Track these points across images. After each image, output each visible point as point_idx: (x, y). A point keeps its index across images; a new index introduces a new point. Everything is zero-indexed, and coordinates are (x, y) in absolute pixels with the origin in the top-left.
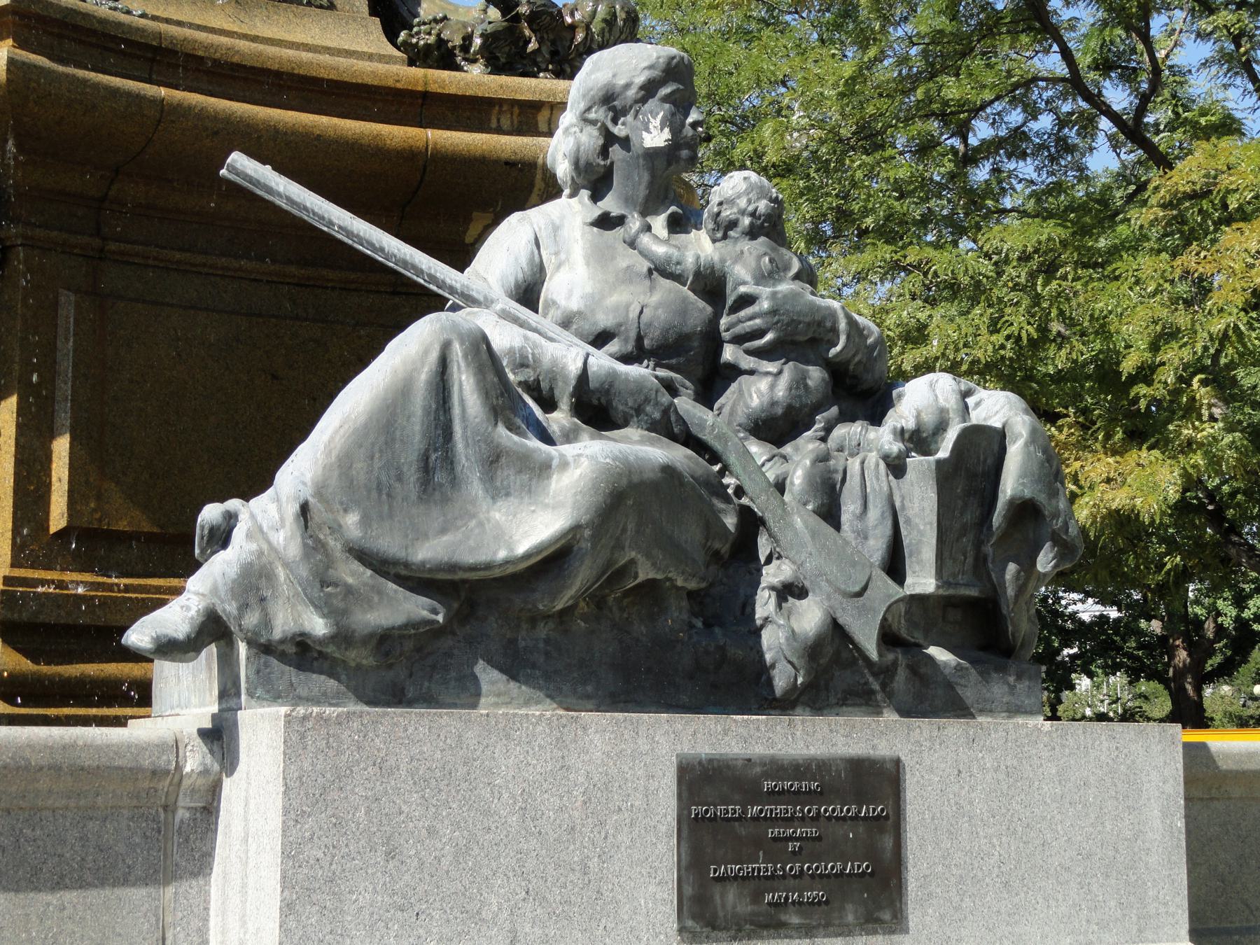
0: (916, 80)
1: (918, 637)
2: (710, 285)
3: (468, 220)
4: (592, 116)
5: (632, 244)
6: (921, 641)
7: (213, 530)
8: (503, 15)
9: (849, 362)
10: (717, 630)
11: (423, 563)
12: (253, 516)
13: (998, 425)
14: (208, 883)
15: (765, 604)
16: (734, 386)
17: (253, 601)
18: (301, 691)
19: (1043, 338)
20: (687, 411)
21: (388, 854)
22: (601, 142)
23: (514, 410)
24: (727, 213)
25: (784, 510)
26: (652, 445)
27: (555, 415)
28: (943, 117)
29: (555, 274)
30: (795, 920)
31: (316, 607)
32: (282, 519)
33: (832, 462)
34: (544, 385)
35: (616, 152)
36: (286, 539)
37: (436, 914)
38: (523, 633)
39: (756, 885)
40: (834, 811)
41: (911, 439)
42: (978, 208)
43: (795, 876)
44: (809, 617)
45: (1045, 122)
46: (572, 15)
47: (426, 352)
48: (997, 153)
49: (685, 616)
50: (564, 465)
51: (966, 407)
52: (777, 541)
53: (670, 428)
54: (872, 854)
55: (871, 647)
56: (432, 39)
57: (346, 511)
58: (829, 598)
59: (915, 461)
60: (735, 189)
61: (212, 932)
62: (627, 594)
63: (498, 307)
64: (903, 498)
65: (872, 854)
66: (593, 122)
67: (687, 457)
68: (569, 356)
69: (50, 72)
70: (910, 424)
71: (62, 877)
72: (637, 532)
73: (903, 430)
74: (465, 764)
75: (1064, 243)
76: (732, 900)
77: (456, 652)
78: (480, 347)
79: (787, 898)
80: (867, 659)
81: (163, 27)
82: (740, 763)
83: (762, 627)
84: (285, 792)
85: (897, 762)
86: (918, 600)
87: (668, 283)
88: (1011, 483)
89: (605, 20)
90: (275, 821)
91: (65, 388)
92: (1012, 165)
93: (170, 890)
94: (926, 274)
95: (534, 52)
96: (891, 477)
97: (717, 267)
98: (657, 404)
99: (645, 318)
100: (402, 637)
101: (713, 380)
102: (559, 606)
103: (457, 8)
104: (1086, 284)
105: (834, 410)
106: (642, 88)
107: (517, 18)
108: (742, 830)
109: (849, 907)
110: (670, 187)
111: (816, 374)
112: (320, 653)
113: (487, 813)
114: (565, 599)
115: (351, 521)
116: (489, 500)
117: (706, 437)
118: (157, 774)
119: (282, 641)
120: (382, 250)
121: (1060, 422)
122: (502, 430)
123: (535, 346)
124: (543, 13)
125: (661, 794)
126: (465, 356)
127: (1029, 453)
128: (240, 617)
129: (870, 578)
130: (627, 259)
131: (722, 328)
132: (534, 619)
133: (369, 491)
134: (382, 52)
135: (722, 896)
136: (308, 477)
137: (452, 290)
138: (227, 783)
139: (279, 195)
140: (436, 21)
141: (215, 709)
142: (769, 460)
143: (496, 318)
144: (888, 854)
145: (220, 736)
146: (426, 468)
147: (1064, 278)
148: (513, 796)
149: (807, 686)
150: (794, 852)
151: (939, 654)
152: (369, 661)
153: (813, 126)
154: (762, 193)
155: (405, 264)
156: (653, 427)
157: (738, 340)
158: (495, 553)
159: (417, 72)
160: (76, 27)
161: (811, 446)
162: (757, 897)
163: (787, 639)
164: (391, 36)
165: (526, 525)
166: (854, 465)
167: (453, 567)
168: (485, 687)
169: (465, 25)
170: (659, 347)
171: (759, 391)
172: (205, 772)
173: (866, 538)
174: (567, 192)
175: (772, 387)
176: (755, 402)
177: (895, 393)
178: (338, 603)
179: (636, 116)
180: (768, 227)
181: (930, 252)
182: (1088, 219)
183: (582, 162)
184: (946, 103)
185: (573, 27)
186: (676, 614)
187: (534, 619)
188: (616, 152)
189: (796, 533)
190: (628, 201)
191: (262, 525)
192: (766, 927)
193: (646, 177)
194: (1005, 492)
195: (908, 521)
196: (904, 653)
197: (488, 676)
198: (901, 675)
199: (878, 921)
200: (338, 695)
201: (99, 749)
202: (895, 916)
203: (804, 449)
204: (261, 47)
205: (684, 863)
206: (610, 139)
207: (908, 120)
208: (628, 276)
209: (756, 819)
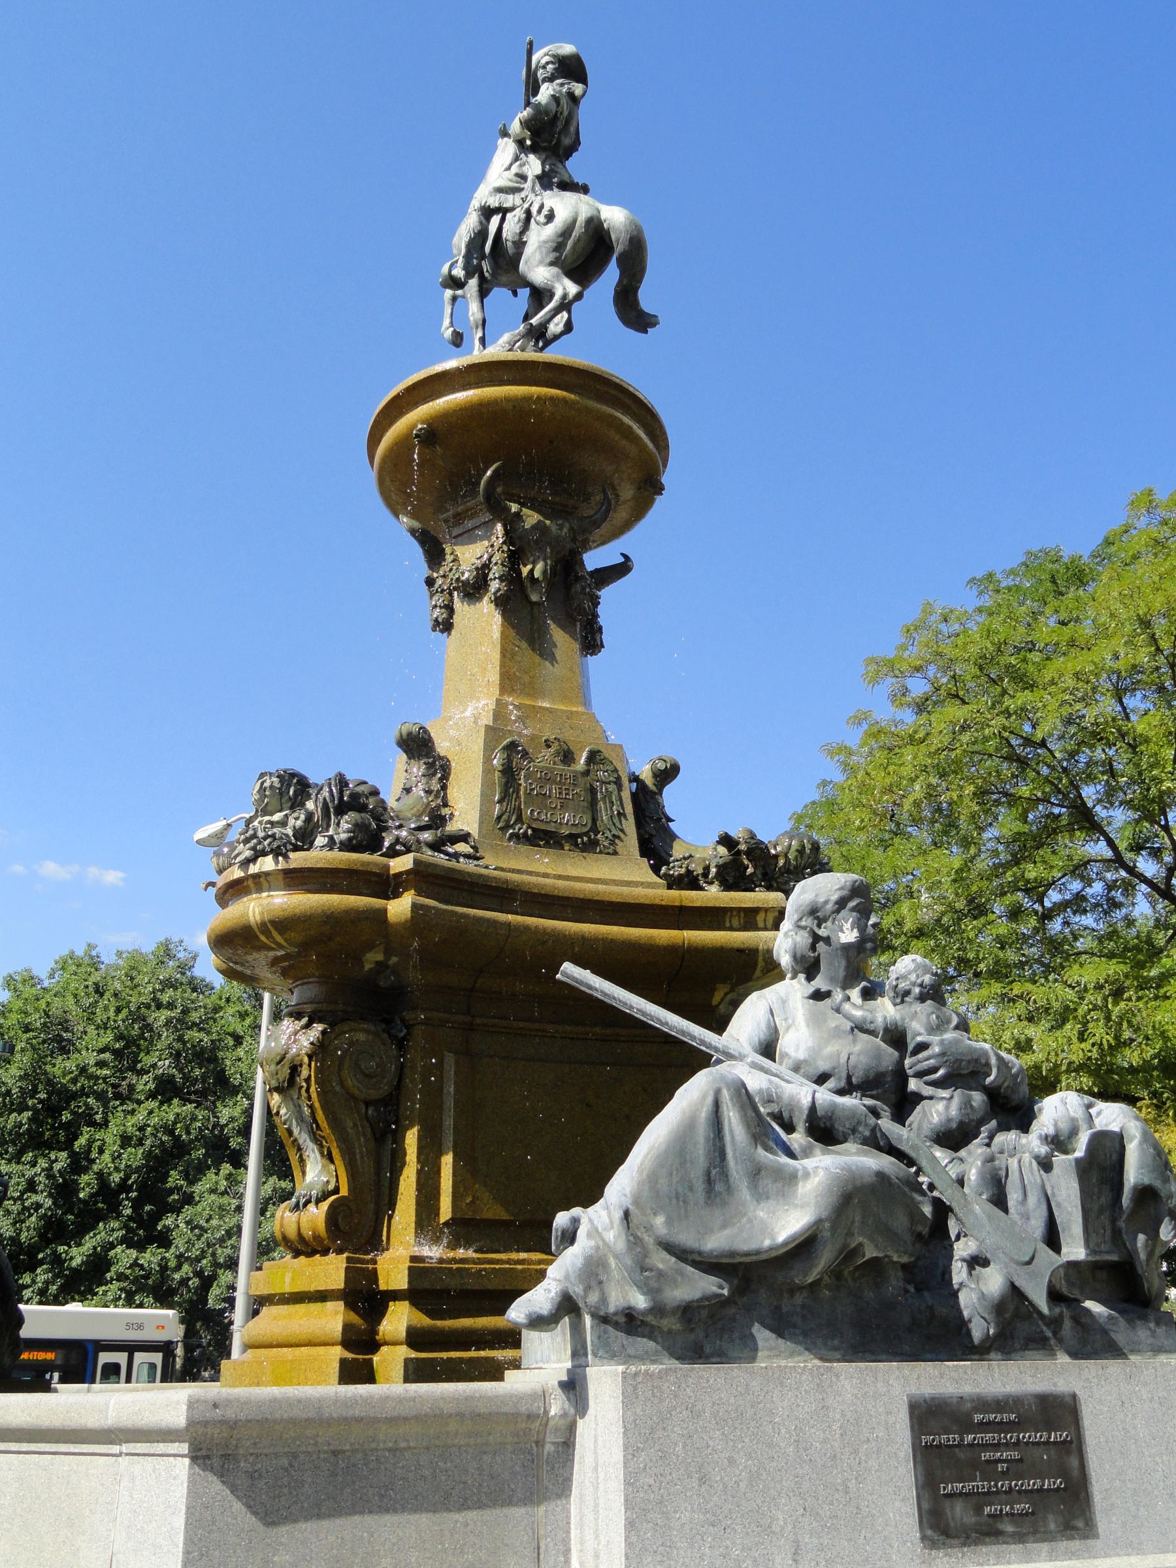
0: (1006, 866)
1: (1076, 1294)
2: (896, 1037)
3: (713, 990)
4: (803, 923)
5: (838, 1010)
6: (1079, 1297)
7: (564, 1232)
8: (729, 851)
9: (1000, 1087)
10: (926, 1293)
11: (711, 1251)
12: (591, 1220)
13: (1117, 1129)
14: (569, 1503)
15: (959, 1273)
16: (919, 1108)
17: (593, 1283)
18: (631, 1351)
19: (1121, 1043)
20: (888, 1129)
21: (700, 1480)
22: (810, 940)
23: (766, 1135)
24: (903, 985)
25: (966, 1200)
26: (866, 1155)
27: (794, 1135)
28: (1027, 891)
29: (785, 1034)
30: (1010, 1529)
31: (638, 1287)
32: (611, 1222)
33: (997, 1162)
34: (786, 1115)
35: (821, 946)
36: (614, 1236)
37: (739, 1528)
38: (785, 1301)
39: (978, 1500)
40: (1030, 1437)
41: (1052, 1142)
42: (1059, 952)
43: (1005, 1492)
44: (993, 1281)
45: (1098, 888)
46: (775, 848)
47: (704, 1097)
48: (1065, 911)
49: (901, 1284)
50: (807, 1175)
51: (1091, 1116)
52: (962, 1223)
53: (879, 1143)
54: (1064, 1473)
55: (1043, 1305)
56: (683, 871)
57: (655, 1214)
58: (1006, 1267)
59: (1059, 1159)
60: (908, 967)
61: (573, 1542)
62: (858, 1268)
63: (749, 1060)
64: (1053, 1188)
65: (1064, 1473)
66: (804, 928)
67: (891, 1163)
68: (802, 1094)
69: (437, 910)
70: (1051, 1131)
71: (466, 1499)
72: (863, 1223)
73: (1046, 1136)
74: (752, 1406)
75: (1126, 976)
76: (959, 1512)
77: (738, 1317)
78: (741, 1092)
79: (1001, 1510)
80: (1039, 1313)
81: (509, 875)
82: (955, 1400)
83: (959, 1290)
84: (624, 1433)
85: (1074, 1396)
86: (1072, 1265)
87: (865, 1037)
88: (1133, 1174)
89: (797, 851)
90: (618, 1455)
91: (449, 1122)
92: (1077, 919)
93: (542, 1508)
94: (1028, 1002)
95: (751, 874)
96: (1042, 1172)
97: (899, 1023)
98: (866, 1125)
99: (851, 1062)
100: (699, 1307)
101: (904, 1105)
102: (810, 1281)
103: (697, 847)
104: (1147, 1003)
105: (994, 1123)
106: (837, 903)
107: (739, 852)
108: (961, 1454)
109: (1051, 1517)
110: (858, 968)
111: (978, 1098)
112: (642, 1321)
113: (770, 1445)
114: (815, 1274)
115: (659, 1221)
116: (755, 1202)
117: (903, 1147)
118: (531, 1417)
119: (616, 1314)
120: (667, 1024)
121: (1138, 1104)
122: (761, 1151)
123: (777, 1087)
124: (757, 848)
125: (898, 1426)
126: (731, 1099)
127: (1143, 1150)
128: (586, 1296)
129: (1035, 1251)
130: (835, 1021)
131: (907, 1066)
132: (793, 1290)
133: (670, 1199)
134: (649, 880)
135: (952, 1508)
136: (628, 1191)
137: (716, 1050)
138: (580, 1423)
139: (596, 990)
140: (685, 858)
141: (569, 1365)
142: (950, 1162)
143: (748, 1068)
144: (1076, 1473)
145: (574, 1386)
146: (709, 1181)
147: (1130, 999)
148: (789, 1432)
149: (998, 1336)
150: (1002, 1472)
151: (1094, 1307)
152: (677, 1326)
153: (936, 904)
154: (926, 970)
155: (683, 1033)
156: (865, 1142)
157: (919, 1075)
158: (762, 1242)
159: (674, 893)
160: (451, 879)
161: (980, 1151)
162: (978, 1510)
163: (979, 1299)
164: (656, 869)
165: (785, 1222)
166: (1013, 1163)
167: (733, 1254)
168: (760, 1344)
169: (704, 860)
170: (863, 1083)
171: (937, 1111)
172: (565, 1415)
173: (1028, 1219)
174: (789, 975)
175: (947, 1108)
176: (936, 1119)
177: (1036, 1108)
178: (653, 1284)
179: (833, 922)
180: (934, 993)
181: (1029, 986)
182: (1140, 957)
183: (798, 955)
184: (1028, 881)
185: (776, 857)
186: (894, 1283)
187: (793, 1290)
188: (821, 946)
189: (976, 1217)
190: (832, 980)
191: (597, 1225)
192: (988, 1534)
193: (844, 963)
194: (1128, 1180)
195: (1059, 1205)
196: (1068, 1307)
197: (762, 1335)
198: (1067, 1324)
199: (1074, 1528)
200: (656, 1353)
201: (490, 1399)
202: (1087, 1524)
203: (975, 1152)
204: (572, 883)
205: (920, 1483)
206: (816, 938)
207: (1003, 894)
208: (837, 1033)
209: (971, 1445)
